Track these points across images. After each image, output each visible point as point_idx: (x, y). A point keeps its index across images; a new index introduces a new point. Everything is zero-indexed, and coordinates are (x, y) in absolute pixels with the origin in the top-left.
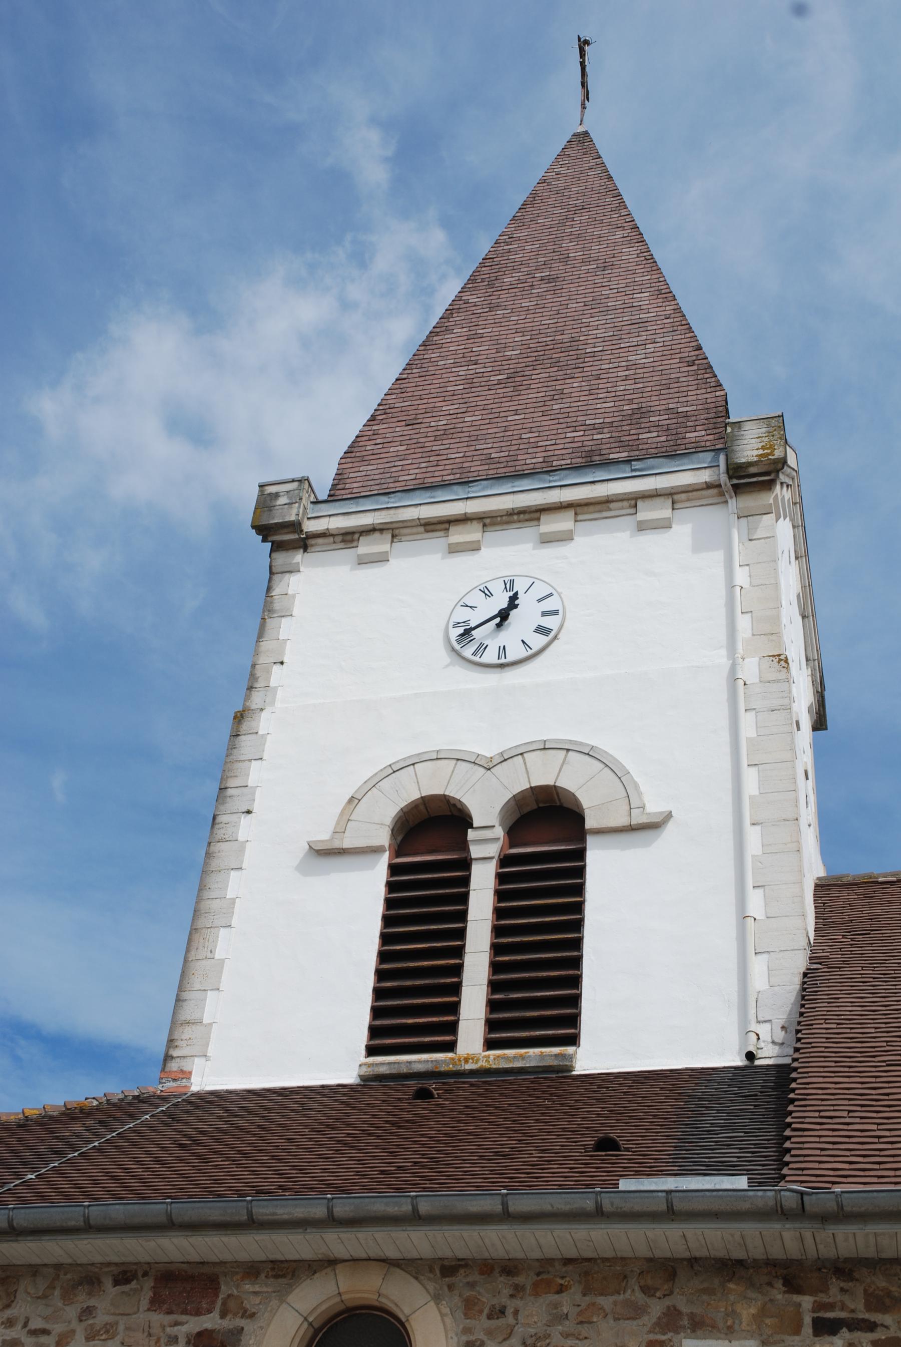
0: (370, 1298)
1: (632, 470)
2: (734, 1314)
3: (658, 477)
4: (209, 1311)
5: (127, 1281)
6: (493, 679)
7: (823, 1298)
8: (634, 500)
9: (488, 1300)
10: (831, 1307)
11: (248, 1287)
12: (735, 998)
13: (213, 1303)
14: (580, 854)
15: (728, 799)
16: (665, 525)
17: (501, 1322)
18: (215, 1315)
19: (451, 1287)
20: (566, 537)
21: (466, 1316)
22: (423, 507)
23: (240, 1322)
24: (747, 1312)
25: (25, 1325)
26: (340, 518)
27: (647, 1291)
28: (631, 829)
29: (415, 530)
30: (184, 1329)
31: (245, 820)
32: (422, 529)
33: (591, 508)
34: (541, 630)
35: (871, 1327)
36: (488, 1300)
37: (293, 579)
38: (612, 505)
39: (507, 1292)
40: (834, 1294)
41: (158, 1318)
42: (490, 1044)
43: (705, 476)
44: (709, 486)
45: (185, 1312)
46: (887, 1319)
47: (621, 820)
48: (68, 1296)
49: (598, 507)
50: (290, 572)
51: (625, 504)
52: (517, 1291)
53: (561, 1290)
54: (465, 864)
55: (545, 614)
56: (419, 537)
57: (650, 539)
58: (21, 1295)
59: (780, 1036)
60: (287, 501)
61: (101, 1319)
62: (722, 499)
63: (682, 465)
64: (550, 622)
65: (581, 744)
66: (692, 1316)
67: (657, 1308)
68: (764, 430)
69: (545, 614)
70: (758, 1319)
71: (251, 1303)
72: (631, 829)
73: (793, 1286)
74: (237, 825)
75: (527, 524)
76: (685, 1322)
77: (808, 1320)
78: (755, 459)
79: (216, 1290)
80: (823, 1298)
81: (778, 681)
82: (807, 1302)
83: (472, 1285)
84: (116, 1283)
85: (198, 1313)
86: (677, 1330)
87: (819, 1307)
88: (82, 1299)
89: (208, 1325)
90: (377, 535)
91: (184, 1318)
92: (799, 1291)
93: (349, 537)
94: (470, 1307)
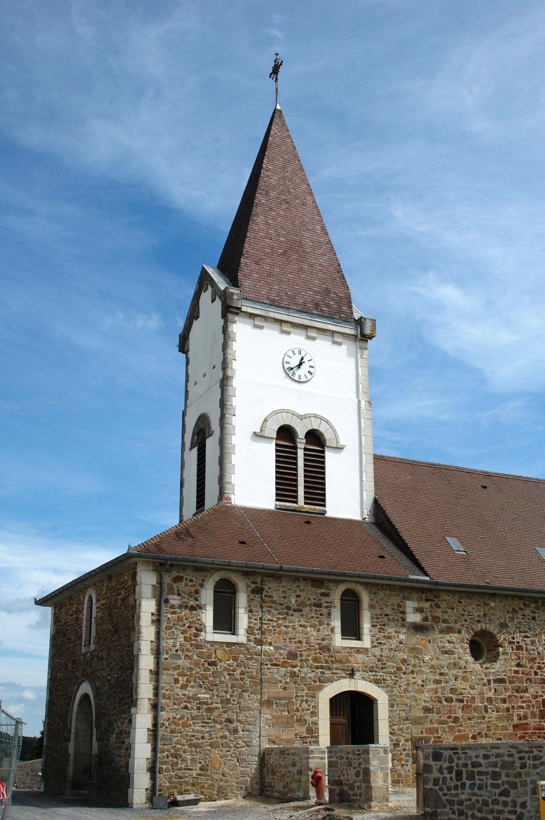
0: (352, 588)
1: (334, 322)
2: (413, 597)
3: (341, 328)
4: (323, 588)
5: (305, 580)
6: (296, 385)
7: (427, 595)
8: (333, 333)
9: (373, 591)
10: (427, 597)
11: (330, 584)
12: (359, 501)
13: (323, 587)
14: (323, 452)
15: (357, 444)
16: (340, 344)
17: (376, 595)
18: (324, 589)
19: (367, 588)
20: (314, 339)
21: (370, 593)
22: (276, 313)
23: (330, 591)
24: (416, 597)
25: (286, 587)
26: (250, 308)
27: (400, 592)
28: (337, 448)
29: (271, 320)
30: (319, 591)
31: (234, 418)
32: (273, 320)
33: (321, 330)
34: (310, 372)
35: (433, 601)
36: (373, 591)
37: (235, 326)
38: (327, 332)
39: (377, 590)
40: (428, 595)
41: (313, 589)
42: (305, 503)
43: (353, 332)
44: (353, 335)
45: (318, 588)
46: (436, 600)
47: (335, 445)
48: (294, 582)
49: (323, 331)
50: (233, 323)
51: (331, 333)
52: (378, 590)
53: (386, 590)
54: (295, 448)
55: (294, 354)
56: (272, 322)
57: (336, 347)
58: (283, 581)
59: (369, 513)
60: (237, 298)
61: (302, 588)
62: (355, 340)
63: (347, 325)
64: (312, 370)
65: (325, 418)
66: (407, 597)
67: (402, 595)
68: (371, 324)
69: (294, 354)
70: (417, 598)
71: (331, 587)
72: (337, 448)
73: (422, 593)
74: (231, 419)
75: (303, 329)
76: (406, 598)
77: (424, 599)
78: (369, 334)
79: (324, 584)
80: (427, 595)
81: (369, 410)
82: (424, 595)
83: (370, 587)
84: (303, 580)
85: (321, 588)
86: (405, 599)
87: (426, 596)
88: (297, 584)
89: (323, 591)
90: (260, 318)
91: (318, 589)
92: (423, 593)
93: (251, 315)
94: (370, 592)
